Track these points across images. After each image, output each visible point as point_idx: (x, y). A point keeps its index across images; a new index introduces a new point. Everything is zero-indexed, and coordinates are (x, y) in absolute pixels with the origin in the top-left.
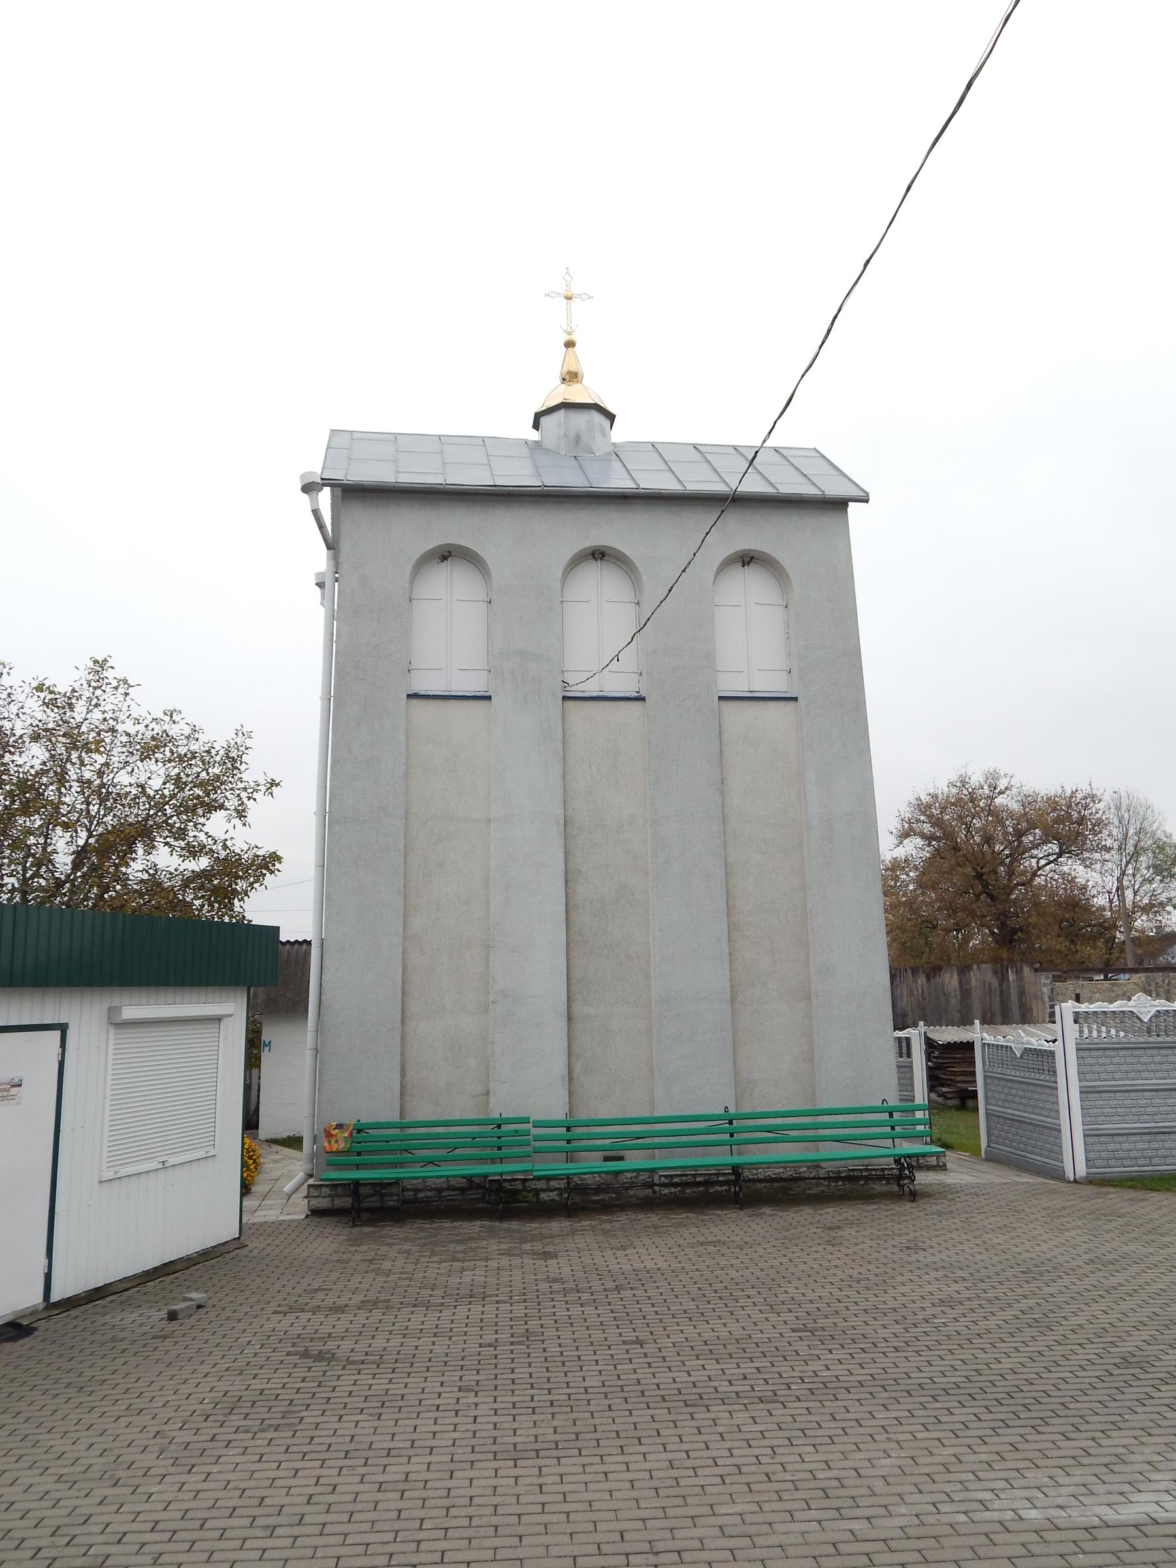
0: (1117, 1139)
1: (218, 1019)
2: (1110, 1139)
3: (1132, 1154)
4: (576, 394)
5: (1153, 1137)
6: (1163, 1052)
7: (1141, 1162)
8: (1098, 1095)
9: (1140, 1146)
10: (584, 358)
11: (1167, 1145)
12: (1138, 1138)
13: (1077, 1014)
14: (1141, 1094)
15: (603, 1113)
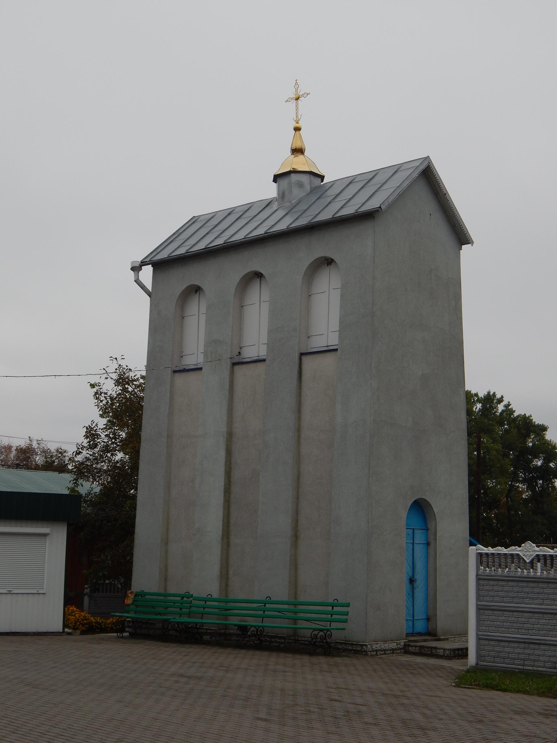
0: (503, 644)
1: (45, 535)
2: (497, 643)
3: (511, 656)
4: (300, 163)
5: (527, 645)
6: (541, 585)
7: (516, 662)
8: (492, 612)
9: (517, 651)
10: (308, 140)
11: (536, 652)
12: (516, 645)
13: (480, 555)
14: (521, 614)
15: (240, 597)
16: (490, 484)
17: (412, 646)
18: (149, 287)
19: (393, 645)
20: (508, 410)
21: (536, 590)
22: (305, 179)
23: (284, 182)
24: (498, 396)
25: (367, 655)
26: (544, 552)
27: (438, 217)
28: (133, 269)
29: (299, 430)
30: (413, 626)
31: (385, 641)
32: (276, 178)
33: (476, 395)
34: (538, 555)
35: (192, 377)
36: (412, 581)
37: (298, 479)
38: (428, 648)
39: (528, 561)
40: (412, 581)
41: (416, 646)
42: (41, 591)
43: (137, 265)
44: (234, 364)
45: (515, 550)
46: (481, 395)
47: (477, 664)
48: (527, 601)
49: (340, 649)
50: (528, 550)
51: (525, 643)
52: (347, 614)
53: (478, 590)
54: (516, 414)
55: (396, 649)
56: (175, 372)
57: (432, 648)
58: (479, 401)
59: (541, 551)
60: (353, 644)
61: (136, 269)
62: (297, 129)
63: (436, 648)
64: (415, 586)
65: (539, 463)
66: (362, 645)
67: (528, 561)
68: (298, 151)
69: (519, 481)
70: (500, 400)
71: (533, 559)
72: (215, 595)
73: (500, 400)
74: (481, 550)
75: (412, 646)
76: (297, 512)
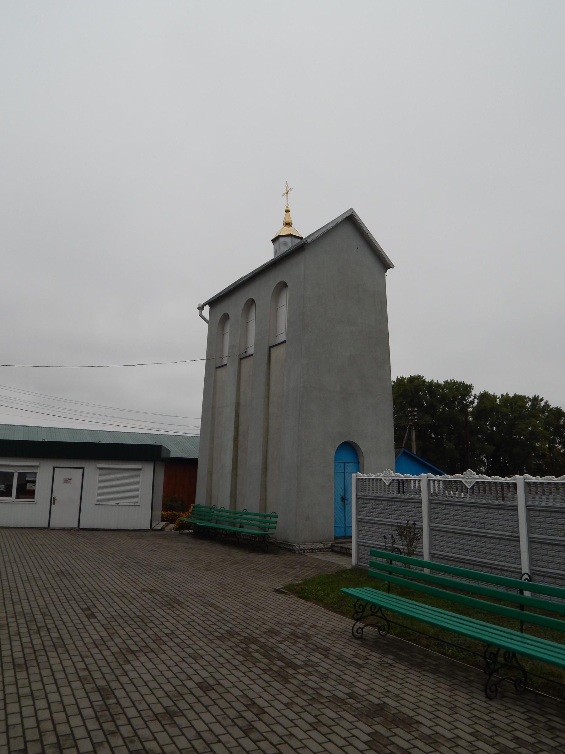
10: (293, 217)
13: (528, 484)
16: (538, 445)
18: (208, 318)
19: (321, 546)
20: (547, 405)
21: (393, 508)
22: (288, 240)
23: (277, 243)
24: (541, 397)
25: (295, 553)
26: (483, 479)
27: (364, 249)
28: (198, 308)
29: (268, 397)
30: (345, 531)
31: (313, 543)
32: (274, 241)
33: (528, 398)
34: (477, 482)
35: (224, 369)
37: (268, 429)
41: (338, 547)
42: (136, 504)
43: (201, 306)
44: (241, 359)
45: (458, 477)
46: (531, 397)
47: (357, 564)
48: (388, 516)
50: (469, 477)
52: (276, 523)
53: (358, 507)
54: (551, 407)
55: (323, 549)
56: (217, 368)
58: (530, 400)
59: (480, 478)
61: (201, 308)
62: (287, 211)
64: (346, 503)
66: (293, 546)
68: (288, 224)
69: (557, 443)
70: (542, 400)
71: (473, 486)
72: (227, 508)
73: (542, 400)
74: (529, 479)
76: (266, 452)
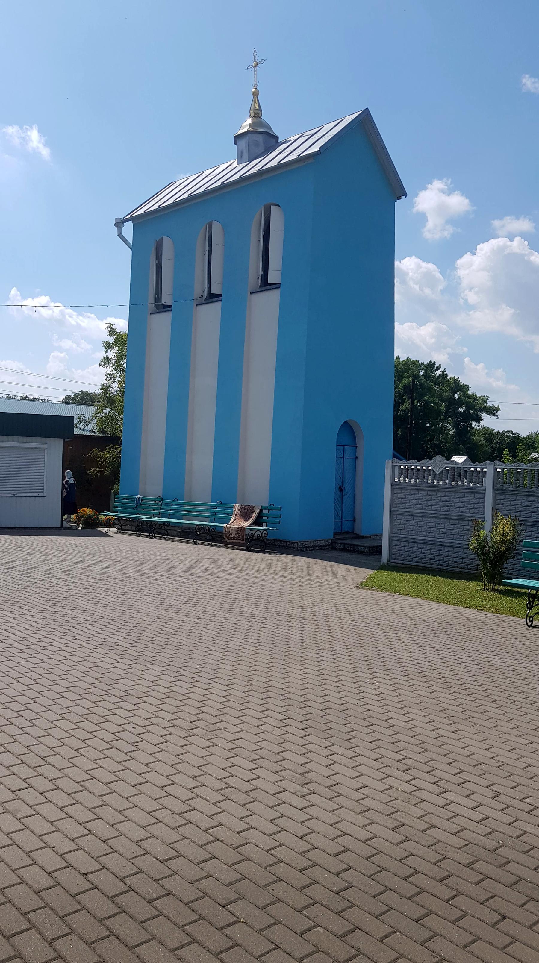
1: (44, 449)
17: (338, 543)
20: (443, 376)
28: (116, 225)
36: (341, 489)
38: (351, 545)
39: (437, 473)
40: (341, 489)
41: (341, 544)
47: (389, 561)
49: (276, 545)
51: (431, 544)
55: (324, 546)
57: (354, 545)
60: (286, 542)
63: (357, 546)
65: (462, 410)
67: (437, 473)
73: (438, 368)
75: (338, 543)
